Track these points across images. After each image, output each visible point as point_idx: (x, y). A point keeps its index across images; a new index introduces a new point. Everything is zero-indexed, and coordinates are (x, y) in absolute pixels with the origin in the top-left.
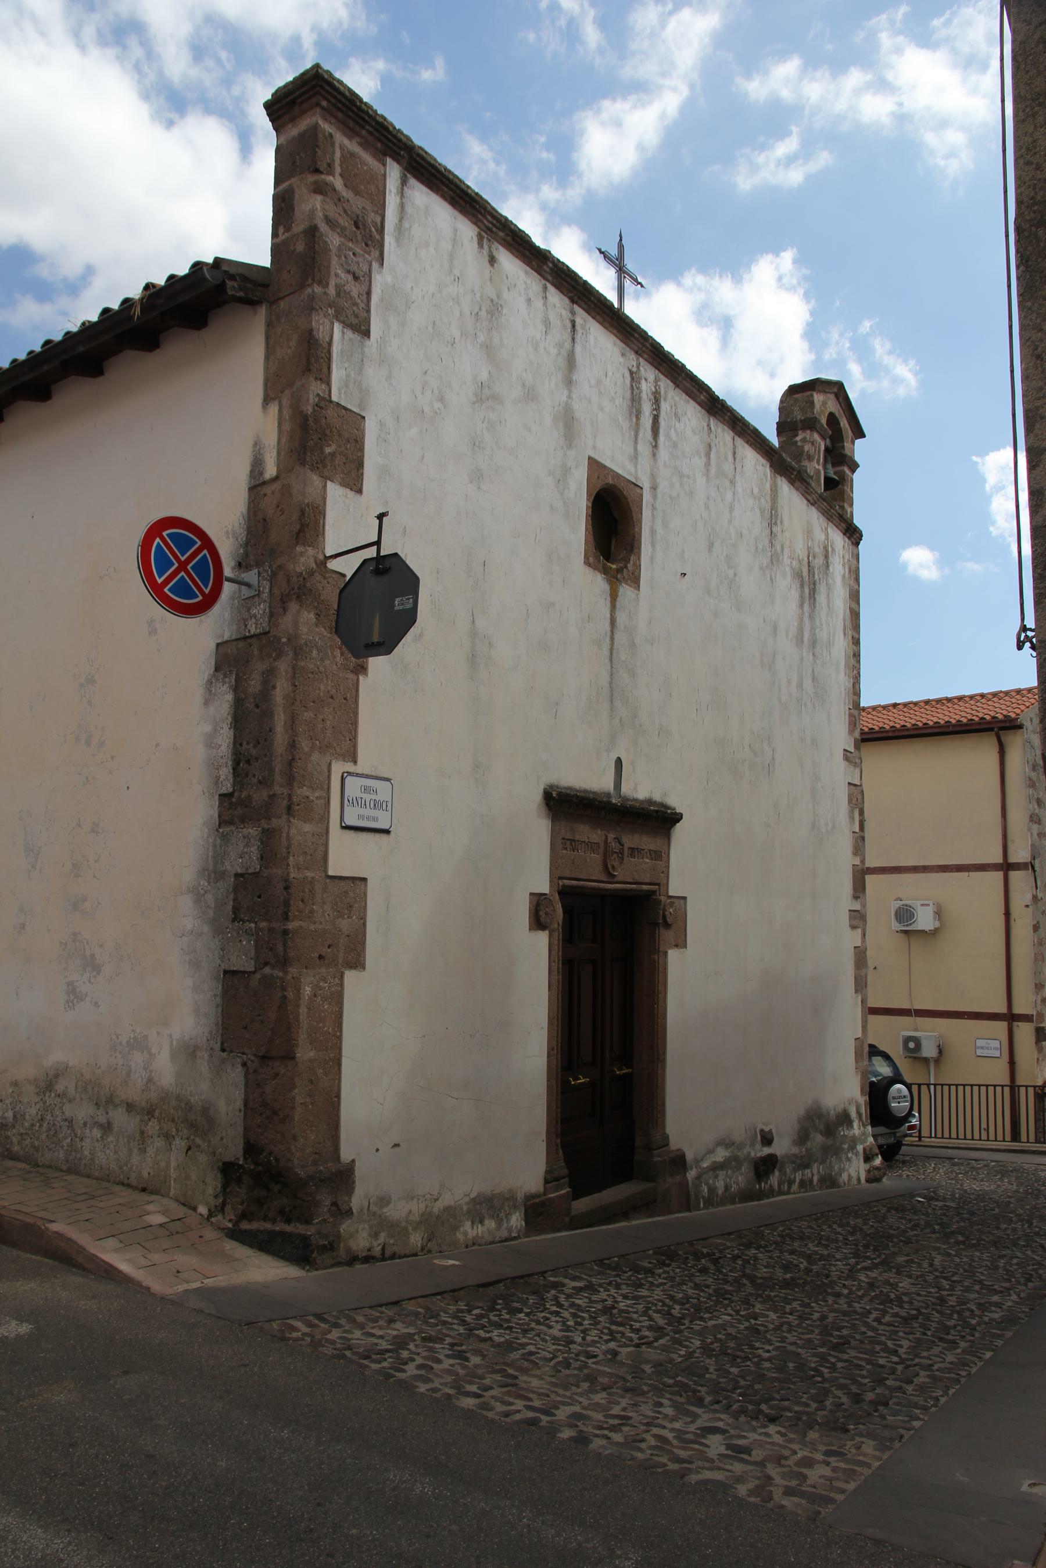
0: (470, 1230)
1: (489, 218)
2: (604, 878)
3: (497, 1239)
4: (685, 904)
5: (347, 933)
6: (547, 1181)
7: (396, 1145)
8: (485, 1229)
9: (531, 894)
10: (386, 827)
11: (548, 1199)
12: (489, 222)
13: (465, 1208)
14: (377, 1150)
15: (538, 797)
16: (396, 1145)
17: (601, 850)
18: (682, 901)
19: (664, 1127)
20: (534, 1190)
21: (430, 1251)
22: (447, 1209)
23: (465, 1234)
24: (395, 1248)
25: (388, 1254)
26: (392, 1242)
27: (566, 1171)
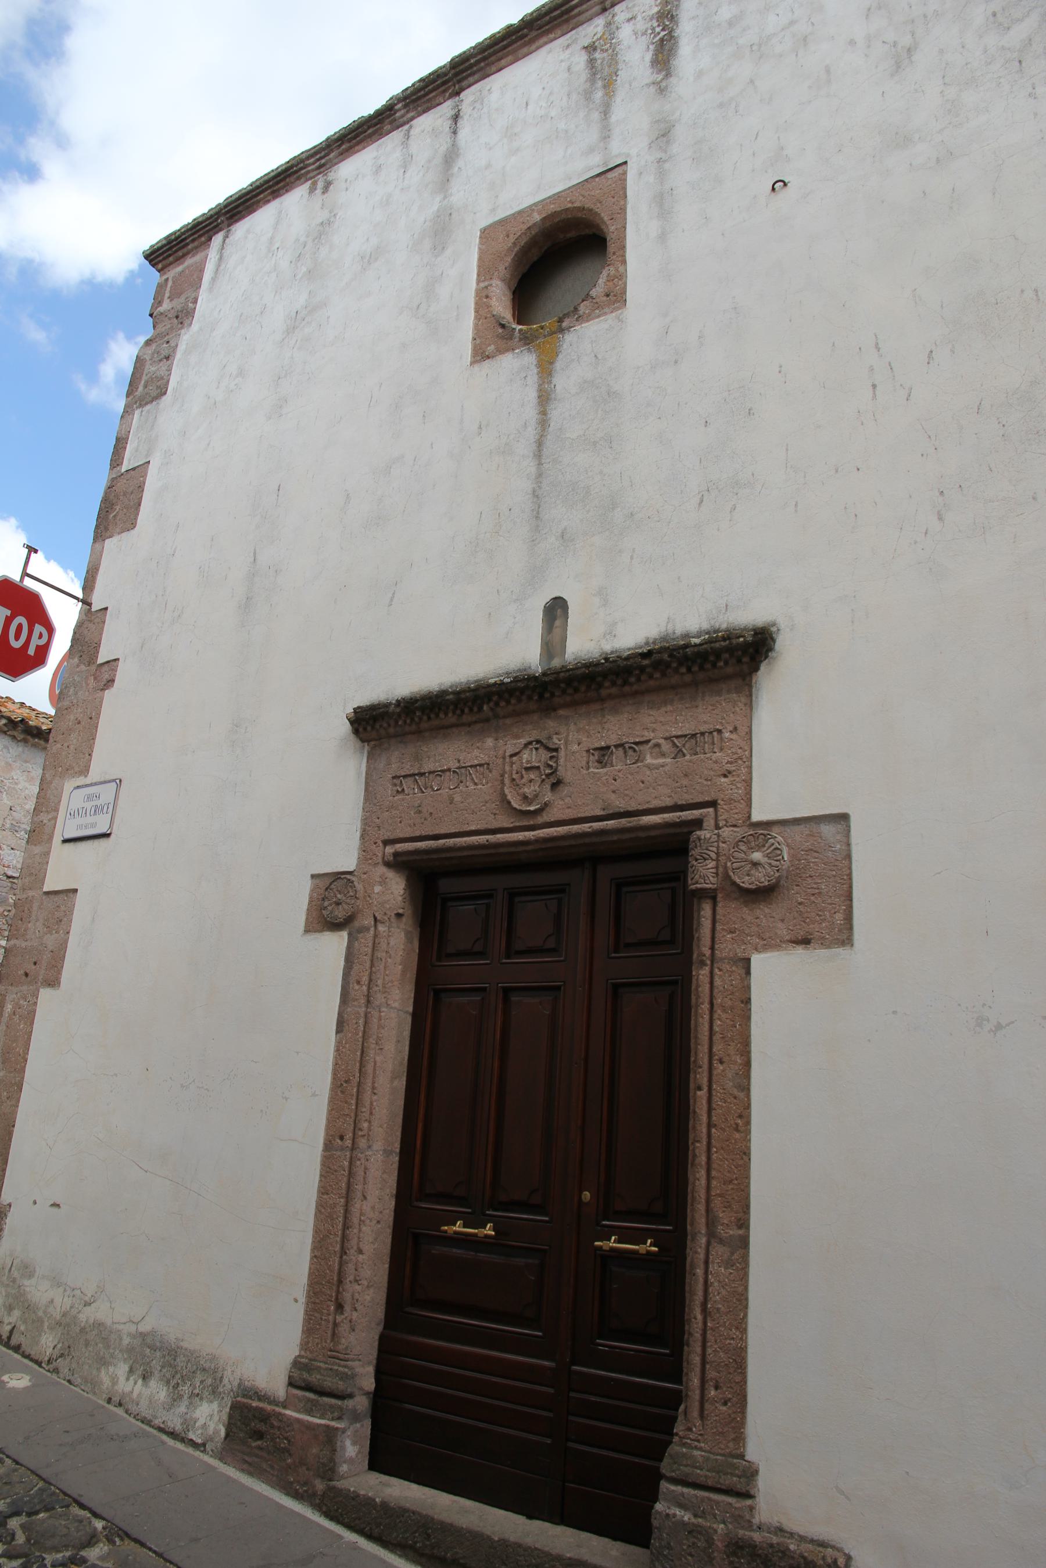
0: (117, 1376)
1: (312, 161)
2: (505, 822)
3: (157, 1422)
5: (51, 948)
6: (291, 1384)
7: (55, 1205)
8: (147, 1392)
9: (313, 876)
10: (103, 829)
12: (314, 163)
13: (126, 1341)
14: (35, 1203)
16: (55, 1205)
17: (495, 774)
18: (828, 830)
21: (56, 1371)
22: (99, 1325)
23: (114, 1381)
24: (22, 1339)
25: (14, 1342)
26: (22, 1328)
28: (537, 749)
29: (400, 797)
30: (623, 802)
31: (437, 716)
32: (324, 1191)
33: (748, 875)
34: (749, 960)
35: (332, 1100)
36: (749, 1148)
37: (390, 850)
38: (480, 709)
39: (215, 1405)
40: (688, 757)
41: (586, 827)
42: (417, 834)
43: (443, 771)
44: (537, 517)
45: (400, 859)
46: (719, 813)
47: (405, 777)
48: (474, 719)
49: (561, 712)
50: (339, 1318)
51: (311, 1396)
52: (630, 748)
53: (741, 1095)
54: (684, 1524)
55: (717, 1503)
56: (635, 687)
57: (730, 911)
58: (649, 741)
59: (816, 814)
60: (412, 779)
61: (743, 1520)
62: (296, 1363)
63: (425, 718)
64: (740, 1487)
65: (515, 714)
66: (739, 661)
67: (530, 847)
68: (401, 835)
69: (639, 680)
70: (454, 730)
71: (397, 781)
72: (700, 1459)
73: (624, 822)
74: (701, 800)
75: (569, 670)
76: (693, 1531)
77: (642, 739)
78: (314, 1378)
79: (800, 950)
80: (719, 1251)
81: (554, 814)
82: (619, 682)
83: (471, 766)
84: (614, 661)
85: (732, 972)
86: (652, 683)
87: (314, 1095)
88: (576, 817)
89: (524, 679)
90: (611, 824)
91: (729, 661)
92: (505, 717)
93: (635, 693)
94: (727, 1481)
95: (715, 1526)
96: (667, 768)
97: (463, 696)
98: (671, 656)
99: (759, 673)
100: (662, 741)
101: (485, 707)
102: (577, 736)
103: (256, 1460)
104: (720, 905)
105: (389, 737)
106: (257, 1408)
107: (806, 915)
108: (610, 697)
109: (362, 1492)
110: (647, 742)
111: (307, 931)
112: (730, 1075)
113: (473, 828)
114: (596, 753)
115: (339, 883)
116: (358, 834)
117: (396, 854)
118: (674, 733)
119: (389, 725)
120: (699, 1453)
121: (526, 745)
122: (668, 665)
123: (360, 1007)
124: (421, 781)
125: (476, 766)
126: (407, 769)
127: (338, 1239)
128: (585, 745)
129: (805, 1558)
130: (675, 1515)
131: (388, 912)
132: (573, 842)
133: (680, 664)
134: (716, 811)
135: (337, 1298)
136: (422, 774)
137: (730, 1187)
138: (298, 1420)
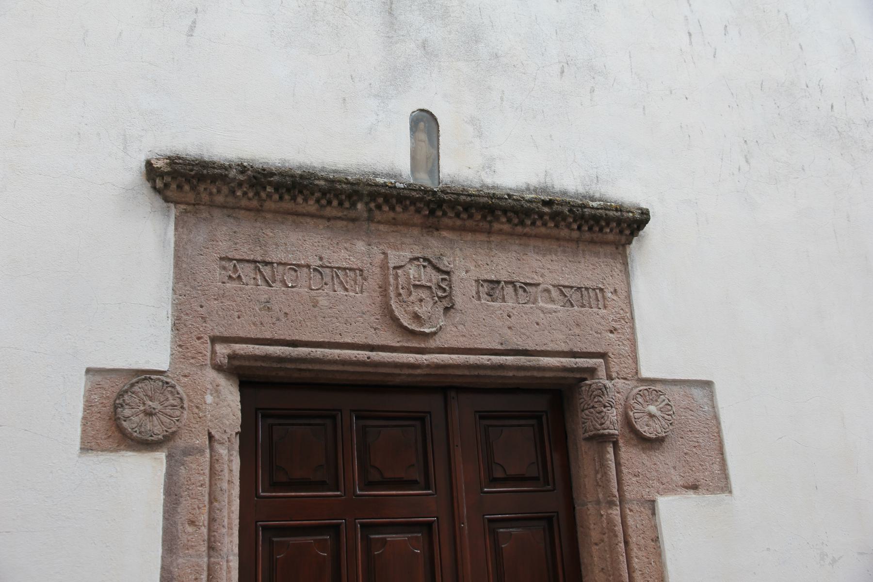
9: (88, 371)
17: (373, 283)
18: (697, 393)
28: (424, 267)
29: (235, 285)
30: (520, 339)
33: (647, 425)
34: (653, 502)
38: (353, 205)
40: (576, 308)
41: (484, 359)
42: (268, 335)
43: (298, 266)
44: (390, 13)
45: (236, 363)
47: (239, 261)
48: (340, 214)
49: (444, 233)
52: (520, 287)
58: (539, 284)
60: (252, 266)
65: (394, 222)
67: (419, 371)
68: (242, 334)
71: (230, 265)
73: (522, 360)
74: (593, 350)
75: (470, 195)
77: (531, 281)
79: (691, 494)
83: (339, 268)
84: (517, 200)
86: (543, 230)
89: (421, 190)
90: (510, 360)
91: (610, 228)
92: (379, 222)
93: (527, 236)
96: (559, 315)
98: (570, 211)
99: (631, 246)
100: (551, 287)
101: (359, 206)
102: (470, 262)
104: (623, 449)
105: (212, 205)
108: (500, 232)
111: (86, 448)
113: (349, 340)
114: (485, 285)
115: (148, 386)
116: (169, 324)
117: (232, 357)
118: (562, 283)
119: (219, 191)
121: (412, 260)
122: (564, 219)
123: (199, 556)
124: (267, 271)
125: (345, 269)
126: (244, 252)
128: (475, 273)
131: (228, 430)
132: (466, 372)
133: (575, 221)
134: (607, 363)
136: (266, 263)
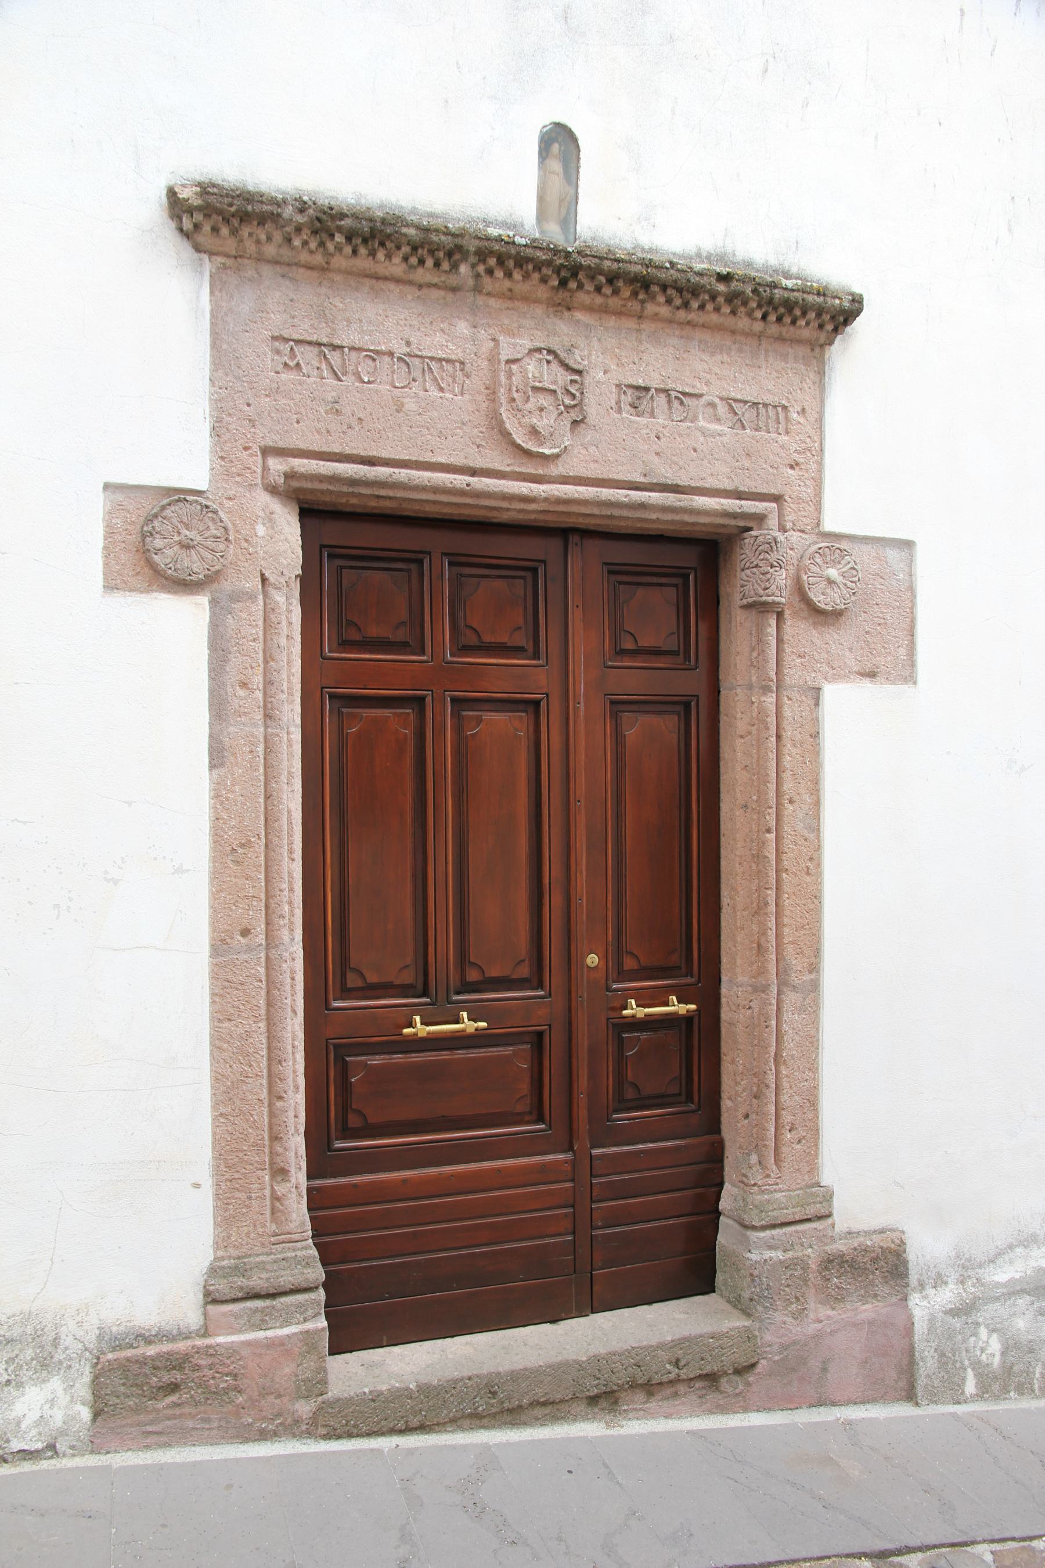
2: (496, 459)
4: (910, 562)
6: (211, 1299)
11: (209, 1352)
15: (152, 208)
17: (477, 382)
18: (893, 555)
19: (811, 1160)
20: (148, 1314)
27: (317, 1273)
28: (548, 362)
31: (373, 254)
32: (221, 1016)
33: (823, 594)
35: (217, 876)
36: (820, 891)
37: (277, 466)
39: (56, 1384)
40: (748, 431)
42: (336, 448)
45: (295, 484)
46: (786, 512)
48: (435, 280)
49: (578, 315)
50: (280, 1189)
51: (259, 1303)
53: (812, 836)
54: (781, 1262)
55: (804, 1232)
56: (692, 316)
57: (796, 629)
59: (877, 535)
60: (315, 350)
61: (823, 1238)
62: (213, 1271)
63: (348, 250)
64: (823, 1211)
65: (510, 296)
66: (821, 327)
67: (533, 507)
69: (702, 307)
70: (392, 286)
72: (784, 1200)
76: (787, 1265)
77: (692, 391)
78: (258, 1281)
79: (867, 683)
80: (791, 998)
81: (575, 465)
82: (678, 302)
83: (432, 358)
85: (802, 701)
87: (179, 870)
88: (605, 477)
90: (654, 497)
91: (804, 318)
92: (489, 294)
94: (811, 1211)
95: (806, 1252)
96: (725, 439)
97: (435, 238)
98: (755, 291)
99: (833, 348)
100: (717, 401)
103: (169, 1423)
104: (789, 623)
105: (260, 259)
106: (159, 1356)
107: (872, 646)
109: (384, 1388)
110: (699, 396)
112: (800, 815)
113: (442, 459)
114: (630, 392)
115: (182, 509)
116: (207, 427)
117: (290, 476)
118: (733, 395)
119: (269, 239)
120: (780, 1194)
123: (255, 725)
124: (334, 357)
125: (440, 360)
126: (304, 330)
127: (265, 1082)
129: (882, 1248)
130: (771, 1259)
134: (780, 510)
135: (272, 1163)
136: (335, 347)
137: (802, 932)
138: (248, 1344)
